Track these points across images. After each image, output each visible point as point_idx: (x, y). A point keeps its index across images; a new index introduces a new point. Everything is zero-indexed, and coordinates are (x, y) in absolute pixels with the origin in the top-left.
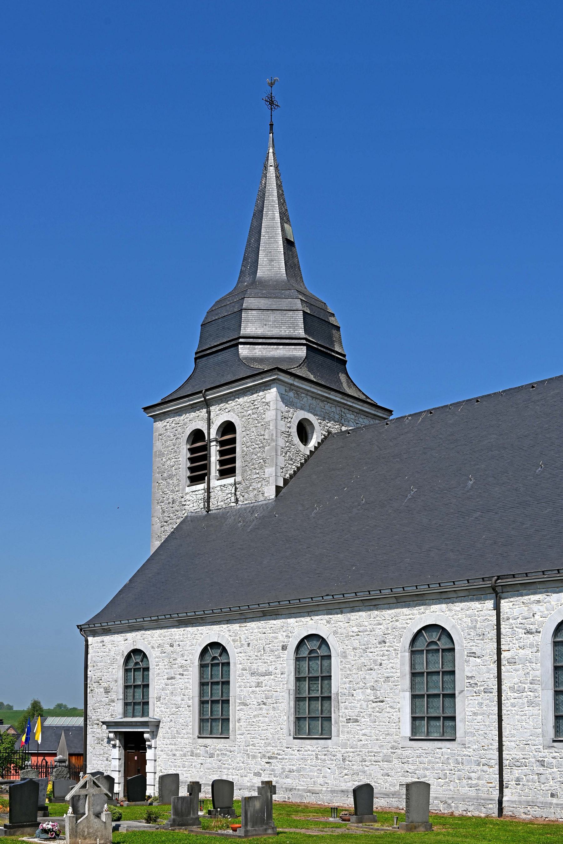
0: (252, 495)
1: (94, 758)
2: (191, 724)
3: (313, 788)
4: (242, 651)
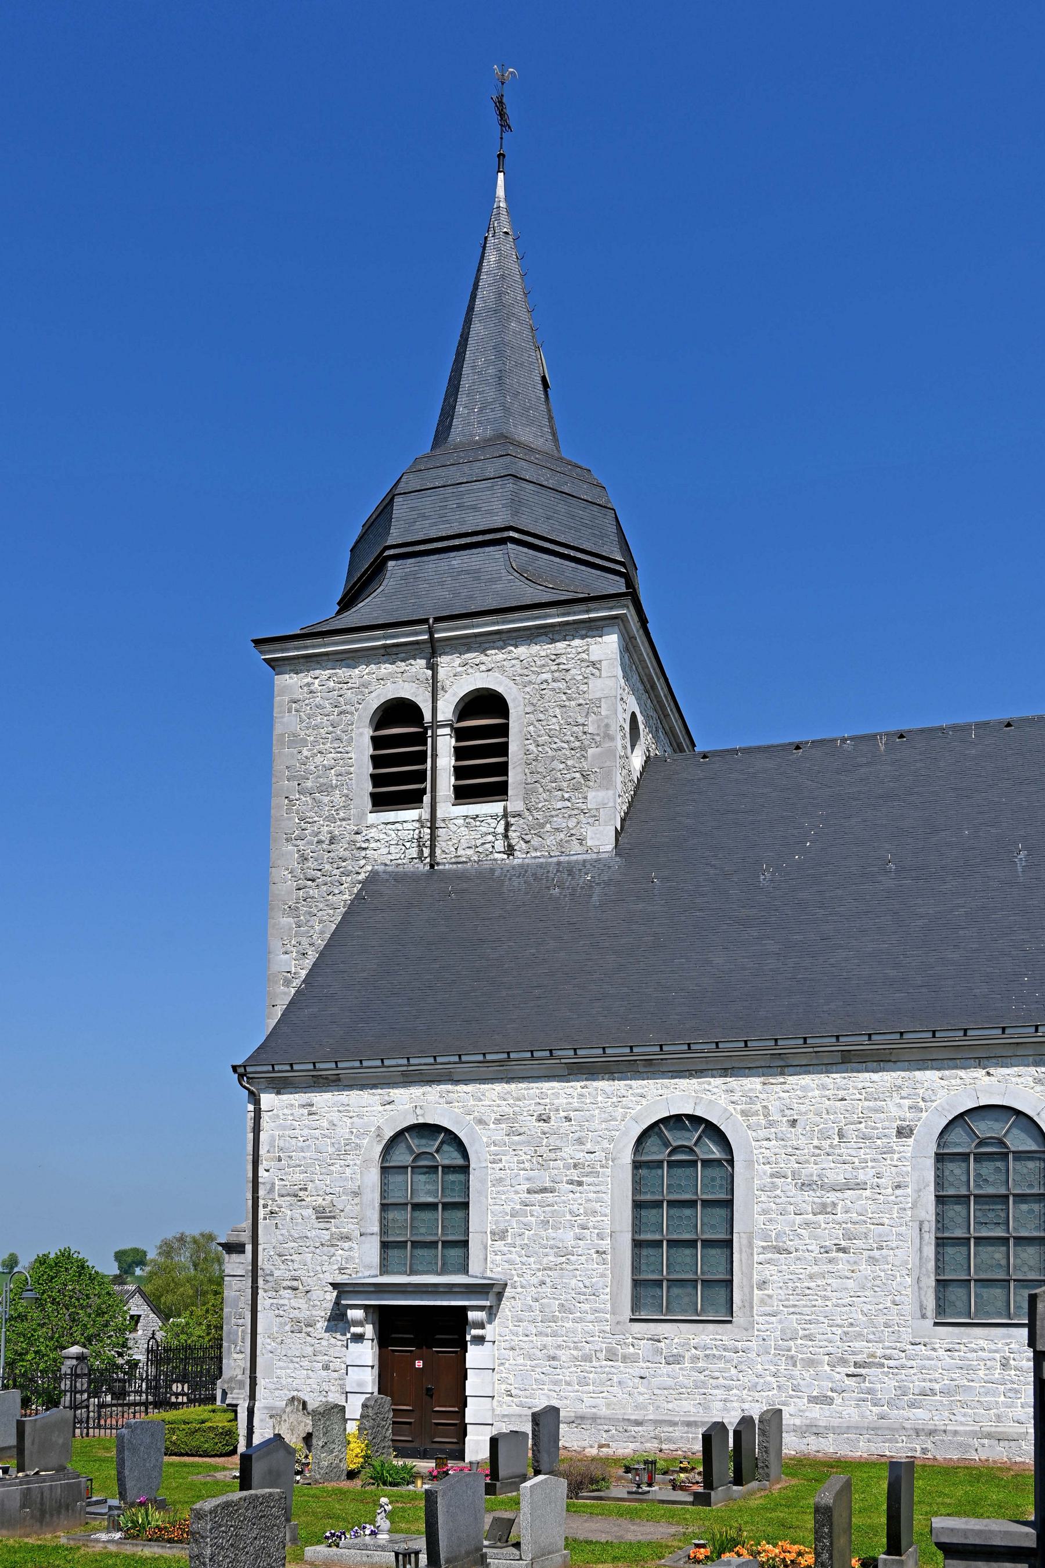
0: (550, 840)
1: (281, 1364)
2: (608, 1290)
3: (999, 1429)
4: (772, 1137)
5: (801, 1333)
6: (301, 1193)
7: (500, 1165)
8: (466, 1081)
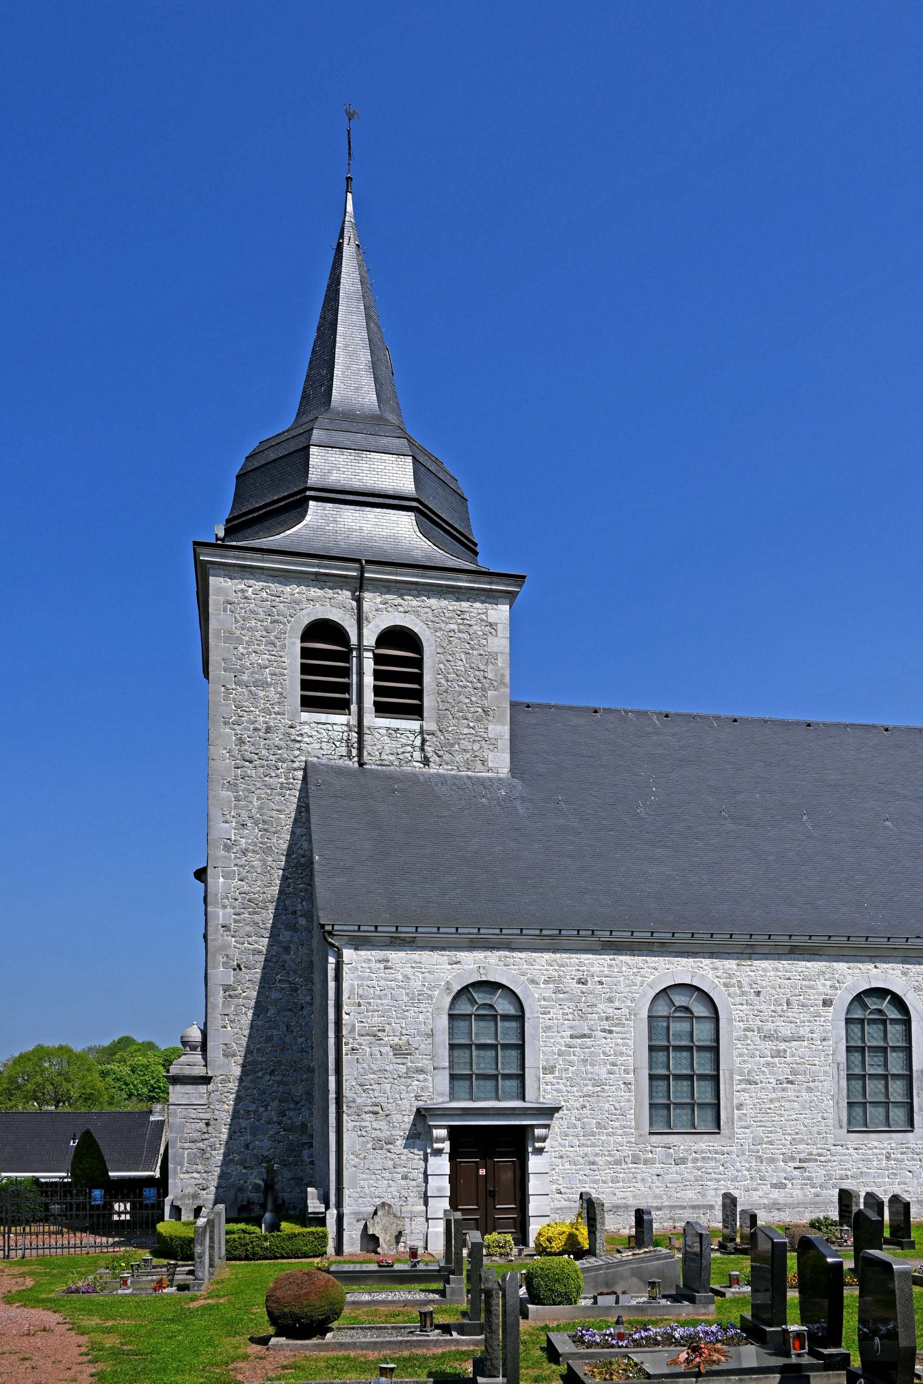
1: (364, 1176)
2: (633, 1111)
5: (765, 1139)
6: (380, 1034)
7: (549, 1016)
8: (521, 950)
